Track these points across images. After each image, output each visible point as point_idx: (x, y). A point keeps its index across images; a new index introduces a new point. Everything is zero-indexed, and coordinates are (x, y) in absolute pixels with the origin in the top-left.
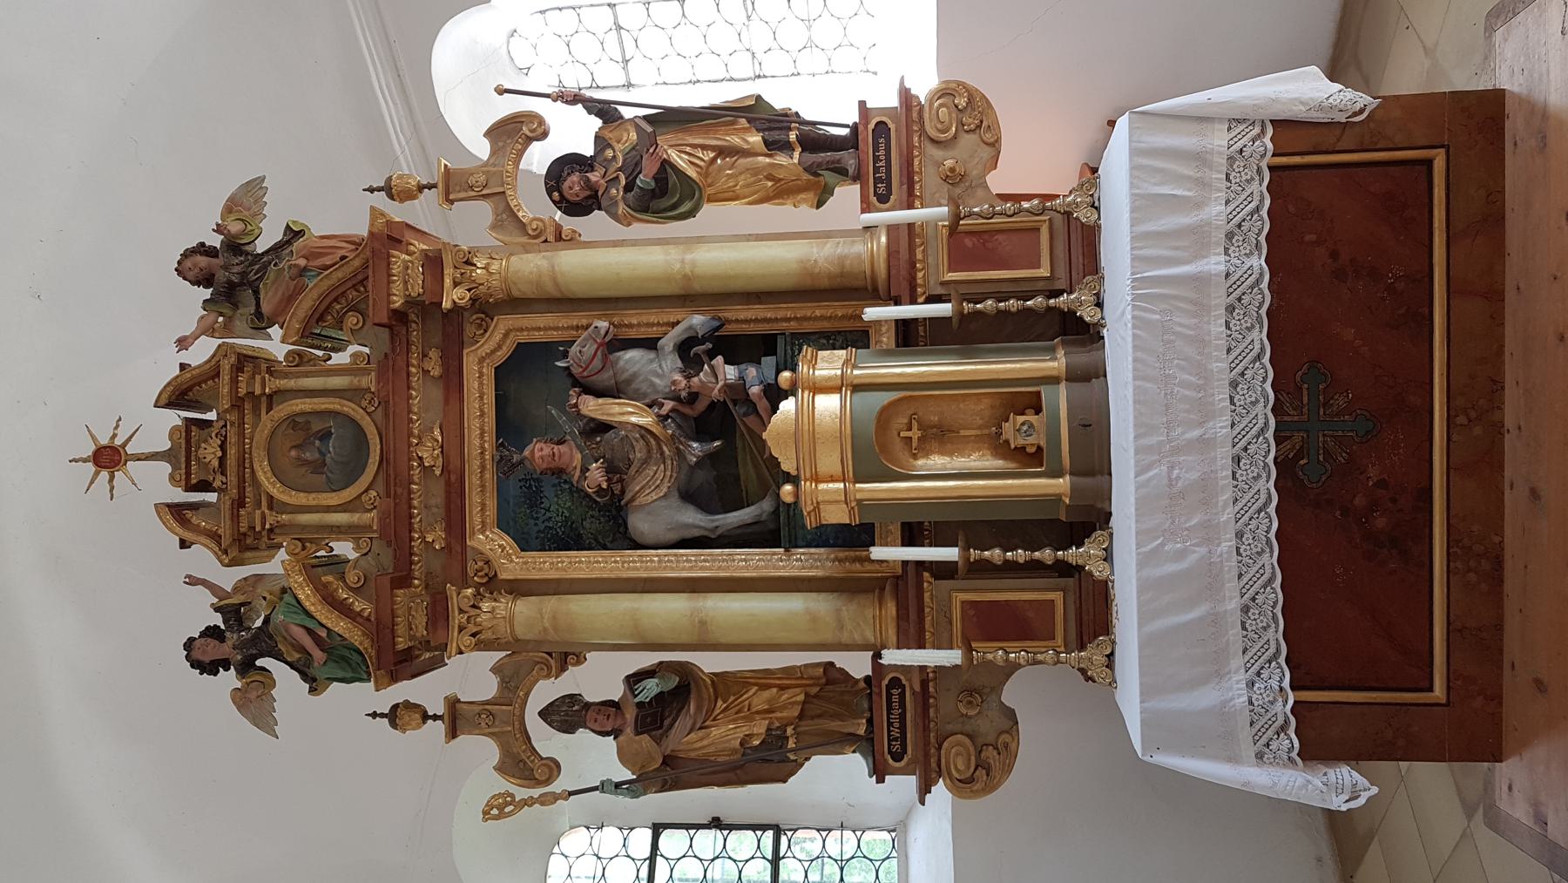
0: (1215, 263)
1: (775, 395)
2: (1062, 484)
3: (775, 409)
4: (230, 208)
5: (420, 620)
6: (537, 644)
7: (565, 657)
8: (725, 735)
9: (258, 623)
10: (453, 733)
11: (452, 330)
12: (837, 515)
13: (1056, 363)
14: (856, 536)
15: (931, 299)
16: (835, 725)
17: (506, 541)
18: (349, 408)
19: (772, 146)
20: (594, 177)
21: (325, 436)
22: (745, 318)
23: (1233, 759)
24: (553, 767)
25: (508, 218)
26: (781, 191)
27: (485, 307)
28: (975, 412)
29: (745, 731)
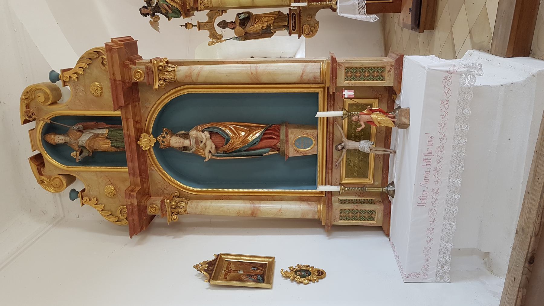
6: (217, 7)
7: (223, 11)
8: (258, 27)
9: (154, 5)
10: (199, 29)
23: (355, 14)
24: (221, 36)
29: (262, 25)
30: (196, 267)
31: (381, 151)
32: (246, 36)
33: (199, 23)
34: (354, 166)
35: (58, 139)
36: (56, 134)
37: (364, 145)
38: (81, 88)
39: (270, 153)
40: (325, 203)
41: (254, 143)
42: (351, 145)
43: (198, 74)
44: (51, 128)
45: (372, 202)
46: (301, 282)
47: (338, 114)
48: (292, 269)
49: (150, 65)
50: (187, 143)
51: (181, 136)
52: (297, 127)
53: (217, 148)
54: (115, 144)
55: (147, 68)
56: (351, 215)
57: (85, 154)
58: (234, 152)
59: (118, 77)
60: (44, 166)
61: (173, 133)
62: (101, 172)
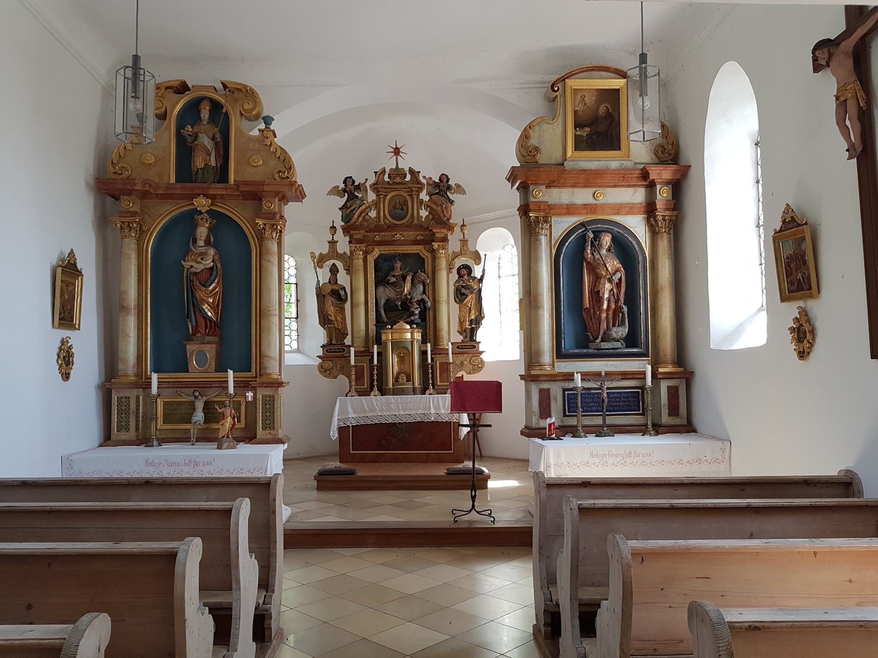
0: (433, 411)
1: (411, 323)
2: (391, 386)
3: (407, 323)
4: (458, 186)
5: (358, 237)
7: (349, 271)
8: (331, 310)
10: (329, 242)
11: (428, 242)
12: (384, 337)
13: (417, 384)
14: (379, 341)
15: (432, 359)
16: (334, 336)
17: (377, 256)
18: (409, 216)
19: (471, 321)
20: (466, 277)
21: (402, 210)
22: (430, 315)
24: (321, 267)
25: (456, 255)
26: (461, 323)
27: (433, 252)
28: (407, 369)
30: (72, 252)
31: (194, 433)
32: (321, 296)
33: (337, 242)
34: (176, 409)
35: (205, 113)
36: (210, 111)
37: (199, 416)
38: (257, 146)
39: (190, 326)
40: (137, 381)
41: (202, 311)
42: (200, 405)
43: (269, 261)
44: (216, 106)
45: (137, 429)
46: (59, 357)
47: (231, 390)
48: (70, 347)
49: (278, 217)
50: (201, 243)
51: (208, 237)
52: (217, 353)
53: (196, 273)
54: (200, 172)
55: (275, 213)
56: (124, 408)
57: (189, 140)
58: (192, 291)
59: (266, 188)
60: (176, 93)
61: (210, 229)
62: (170, 152)
